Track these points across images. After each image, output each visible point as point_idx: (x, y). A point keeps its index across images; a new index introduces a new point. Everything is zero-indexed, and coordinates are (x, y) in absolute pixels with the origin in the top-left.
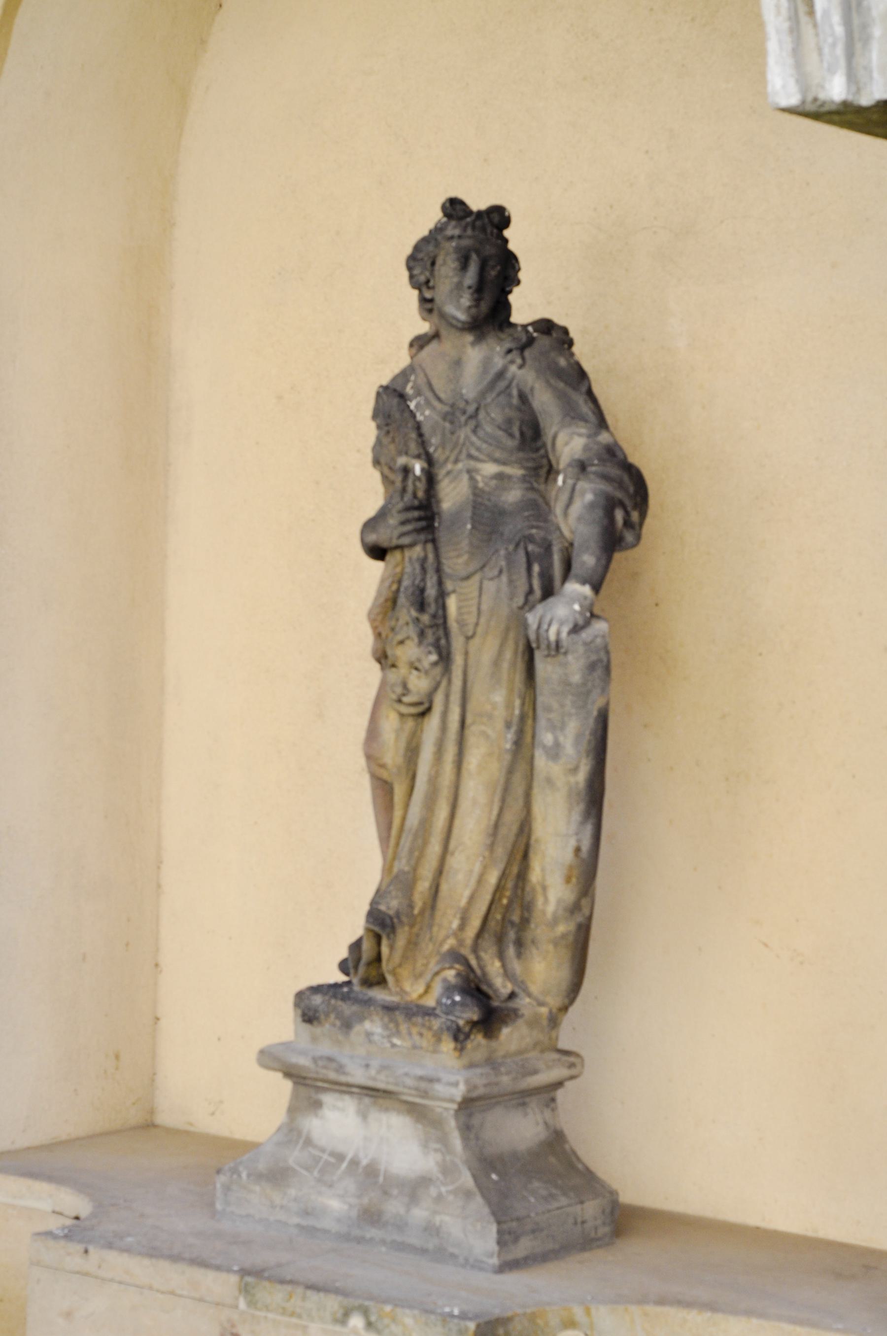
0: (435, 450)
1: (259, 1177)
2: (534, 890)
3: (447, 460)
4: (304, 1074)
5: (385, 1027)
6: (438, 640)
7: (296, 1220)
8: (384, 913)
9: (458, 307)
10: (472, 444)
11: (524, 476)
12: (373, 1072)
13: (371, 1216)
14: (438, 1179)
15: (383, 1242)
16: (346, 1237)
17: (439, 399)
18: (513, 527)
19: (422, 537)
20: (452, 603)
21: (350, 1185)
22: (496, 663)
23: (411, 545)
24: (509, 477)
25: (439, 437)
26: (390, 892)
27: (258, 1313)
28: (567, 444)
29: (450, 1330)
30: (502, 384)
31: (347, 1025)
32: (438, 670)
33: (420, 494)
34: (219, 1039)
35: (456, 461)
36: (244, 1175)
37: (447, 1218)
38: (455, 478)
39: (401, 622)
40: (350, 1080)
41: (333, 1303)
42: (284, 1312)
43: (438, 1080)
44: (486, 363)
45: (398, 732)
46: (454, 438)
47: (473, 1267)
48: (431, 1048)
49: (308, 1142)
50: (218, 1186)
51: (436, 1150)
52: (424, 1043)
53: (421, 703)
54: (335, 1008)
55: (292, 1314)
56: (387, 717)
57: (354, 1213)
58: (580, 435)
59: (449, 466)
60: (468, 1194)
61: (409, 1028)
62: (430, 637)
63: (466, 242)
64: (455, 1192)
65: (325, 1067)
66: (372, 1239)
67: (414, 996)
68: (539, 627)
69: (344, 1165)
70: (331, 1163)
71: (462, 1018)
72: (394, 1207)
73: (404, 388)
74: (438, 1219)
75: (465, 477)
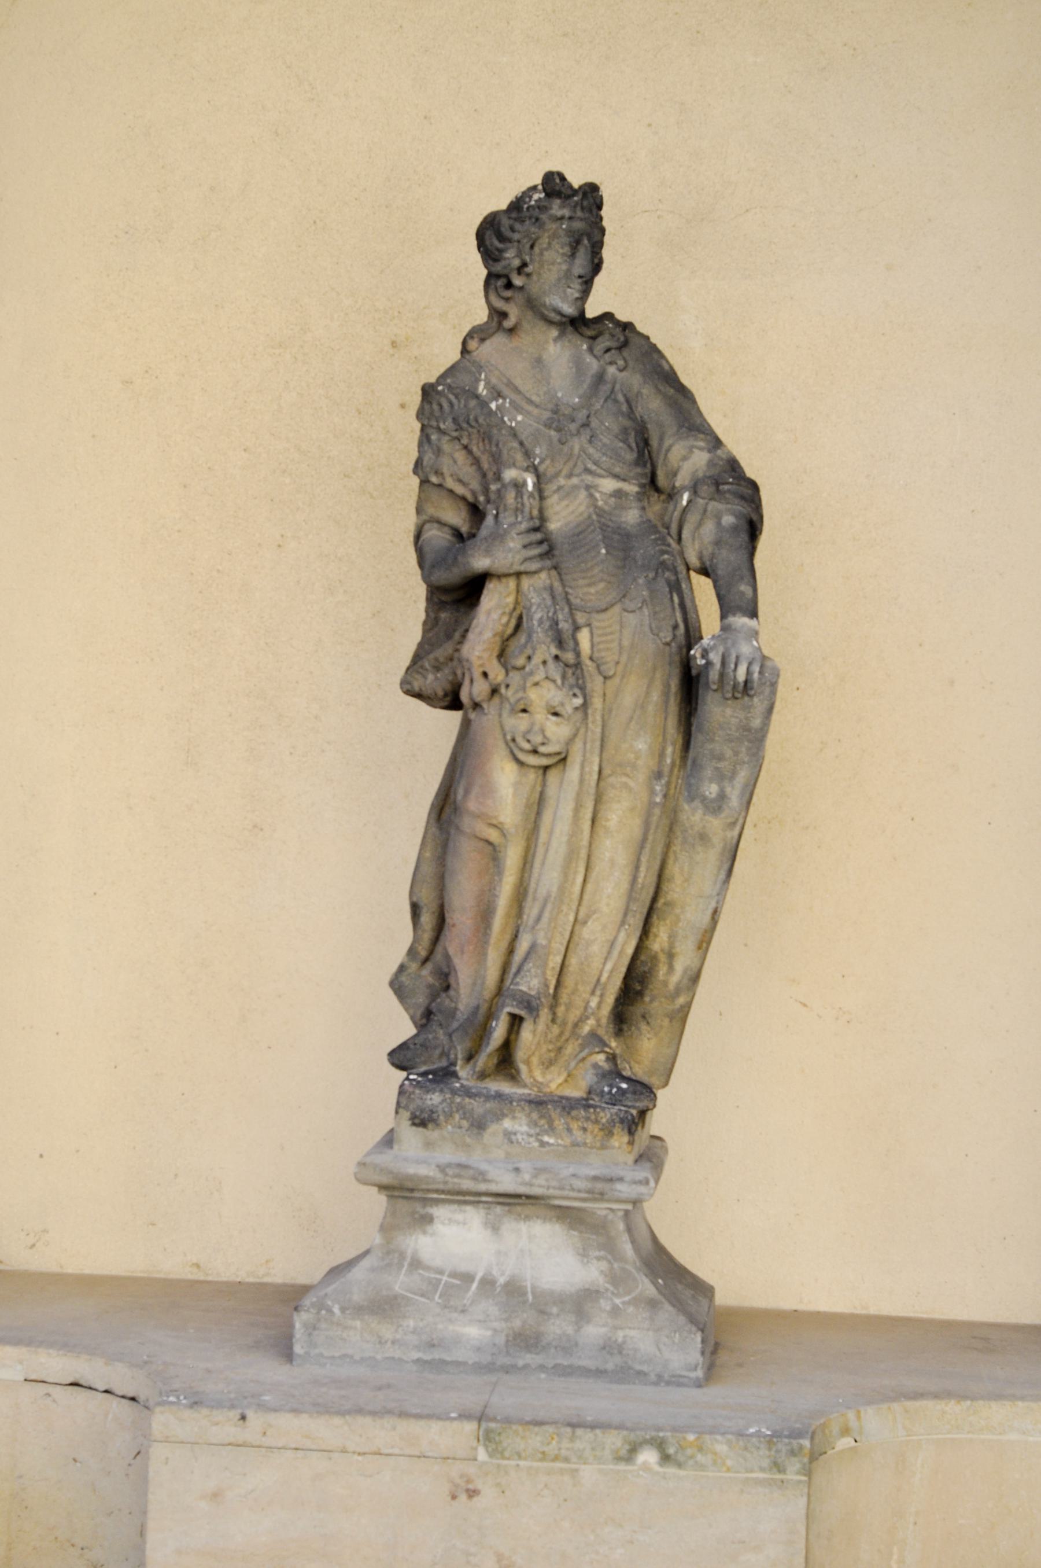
0: (542, 462)
1: (359, 1310)
2: (654, 958)
3: (557, 475)
4: (410, 1185)
7: (415, 1355)
8: (525, 993)
9: (564, 299)
10: (589, 456)
11: (638, 493)
12: (527, 1177)
13: (526, 1340)
14: (607, 1290)
15: (542, 1368)
16: (489, 1368)
17: (530, 402)
18: (644, 550)
19: (548, 563)
20: (584, 637)
21: (490, 1307)
22: (641, 706)
23: (535, 572)
24: (627, 494)
25: (544, 447)
26: (529, 971)
27: (505, 1462)
28: (685, 458)
29: (778, 1451)
31: (479, 1126)
34: (41, 1156)
35: (570, 476)
36: (336, 1310)
37: (632, 1333)
38: (568, 494)
39: (537, 660)
40: (494, 1188)
41: (614, 1441)
42: (544, 1456)
43: (621, 1179)
45: (517, 785)
46: (565, 448)
47: (668, 1383)
48: (598, 1144)
49: (416, 1264)
50: (298, 1325)
51: (598, 1259)
52: (589, 1139)
53: (559, 753)
54: (461, 1107)
55: (556, 1458)
56: (502, 769)
57: (501, 1340)
58: (701, 449)
59: (562, 481)
61: (567, 1124)
63: (578, 225)
65: (458, 1176)
66: (526, 1366)
67: (553, 1086)
68: (724, 663)
69: (475, 1285)
71: (634, 1107)
72: (559, 1326)
73: (477, 388)
74: (620, 1335)
75: (583, 494)
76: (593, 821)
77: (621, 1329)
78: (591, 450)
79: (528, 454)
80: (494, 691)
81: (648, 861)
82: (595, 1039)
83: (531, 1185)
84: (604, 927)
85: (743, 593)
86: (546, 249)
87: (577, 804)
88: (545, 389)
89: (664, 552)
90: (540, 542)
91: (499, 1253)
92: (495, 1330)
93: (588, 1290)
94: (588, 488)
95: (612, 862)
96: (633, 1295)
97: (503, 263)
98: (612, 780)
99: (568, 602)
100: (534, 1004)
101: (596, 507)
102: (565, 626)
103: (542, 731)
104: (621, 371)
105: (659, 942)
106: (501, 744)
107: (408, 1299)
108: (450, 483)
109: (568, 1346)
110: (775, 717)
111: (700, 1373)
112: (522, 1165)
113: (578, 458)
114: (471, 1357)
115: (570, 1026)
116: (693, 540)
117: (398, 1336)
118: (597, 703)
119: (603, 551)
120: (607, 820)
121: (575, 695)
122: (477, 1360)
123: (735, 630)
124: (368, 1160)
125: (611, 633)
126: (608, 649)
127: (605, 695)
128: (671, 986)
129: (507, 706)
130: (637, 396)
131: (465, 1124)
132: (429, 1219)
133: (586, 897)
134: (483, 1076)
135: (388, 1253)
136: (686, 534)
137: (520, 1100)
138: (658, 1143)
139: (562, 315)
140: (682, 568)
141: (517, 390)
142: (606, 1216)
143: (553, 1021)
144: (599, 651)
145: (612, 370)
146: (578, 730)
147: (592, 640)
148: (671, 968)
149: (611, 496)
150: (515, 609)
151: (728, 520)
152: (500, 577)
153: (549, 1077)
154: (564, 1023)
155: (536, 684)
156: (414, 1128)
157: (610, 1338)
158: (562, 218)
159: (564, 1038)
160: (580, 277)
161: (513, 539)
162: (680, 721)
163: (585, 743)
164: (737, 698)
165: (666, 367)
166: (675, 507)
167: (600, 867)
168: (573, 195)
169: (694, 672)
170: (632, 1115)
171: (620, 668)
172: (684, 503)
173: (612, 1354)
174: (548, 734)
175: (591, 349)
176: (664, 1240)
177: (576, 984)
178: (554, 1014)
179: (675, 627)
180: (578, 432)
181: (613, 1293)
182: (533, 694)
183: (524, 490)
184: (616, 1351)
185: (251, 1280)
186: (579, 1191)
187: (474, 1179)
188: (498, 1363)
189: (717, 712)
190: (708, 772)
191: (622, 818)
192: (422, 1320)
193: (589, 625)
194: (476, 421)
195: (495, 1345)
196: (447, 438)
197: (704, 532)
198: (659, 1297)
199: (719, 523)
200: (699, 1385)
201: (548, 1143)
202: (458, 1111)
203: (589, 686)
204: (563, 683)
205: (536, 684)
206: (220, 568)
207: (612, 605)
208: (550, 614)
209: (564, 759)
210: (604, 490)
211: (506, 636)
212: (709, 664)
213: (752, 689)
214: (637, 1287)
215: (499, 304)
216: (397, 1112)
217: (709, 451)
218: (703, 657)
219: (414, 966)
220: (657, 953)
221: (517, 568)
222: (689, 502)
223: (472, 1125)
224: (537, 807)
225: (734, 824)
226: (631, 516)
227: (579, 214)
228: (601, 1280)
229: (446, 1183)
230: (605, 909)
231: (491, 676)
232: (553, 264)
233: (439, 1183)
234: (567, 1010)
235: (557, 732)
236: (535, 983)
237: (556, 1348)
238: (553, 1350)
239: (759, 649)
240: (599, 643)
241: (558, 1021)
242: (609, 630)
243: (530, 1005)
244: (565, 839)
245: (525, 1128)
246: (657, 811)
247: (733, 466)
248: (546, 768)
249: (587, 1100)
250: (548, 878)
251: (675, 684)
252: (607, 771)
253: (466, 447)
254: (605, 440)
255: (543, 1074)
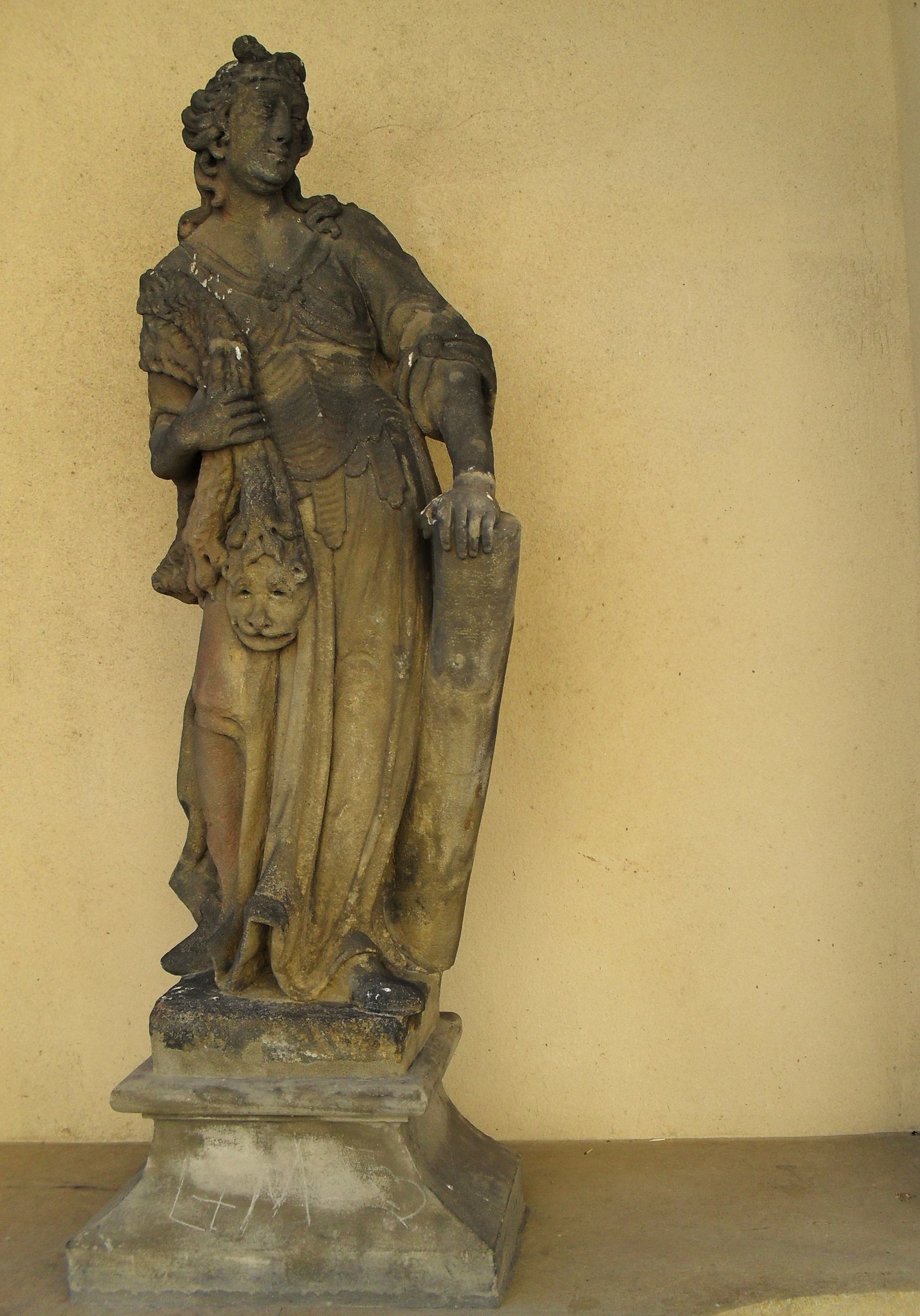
1: (131, 1244)
2: (421, 842)
3: (270, 342)
5: (292, 1039)
6: (300, 553)
7: (194, 1288)
12: (289, 1098)
13: (306, 1268)
14: (389, 1207)
15: (327, 1295)
17: (240, 274)
19: (261, 432)
20: (307, 510)
21: (266, 1233)
23: (248, 443)
24: (348, 359)
26: (274, 874)
28: (408, 320)
30: (319, 256)
31: (236, 1044)
32: (305, 592)
33: (246, 382)
35: (283, 342)
36: (108, 1245)
37: (419, 1255)
43: (389, 1095)
44: (291, 237)
45: (248, 674)
46: (277, 315)
47: (463, 1305)
49: (190, 1188)
50: (71, 1262)
51: (378, 1174)
57: (281, 1268)
58: (424, 309)
59: (275, 349)
60: (438, 1221)
62: (293, 554)
63: (271, 85)
64: (418, 1220)
66: (309, 1294)
67: (315, 993)
68: (454, 520)
69: (251, 1209)
70: (231, 1212)
71: (400, 1013)
72: (339, 1252)
75: (298, 361)
76: (335, 703)
77: (407, 1251)
78: (303, 315)
79: (237, 324)
80: (219, 576)
81: (397, 743)
82: (360, 939)
83: (294, 1107)
84: (357, 817)
85: (475, 448)
86: (242, 114)
87: (312, 689)
88: (256, 261)
89: (389, 414)
90: (252, 411)
91: (274, 1173)
92: (273, 1259)
93: (370, 1208)
94: (302, 353)
95: (360, 748)
96: (418, 1211)
97: (201, 135)
98: (350, 659)
99: (286, 471)
100: (281, 910)
101: (313, 372)
102: (283, 497)
103: (265, 612)
104: (335, 238)
105: (423, 824)
106: (229, 632)
107: (184, 1228)
108: (169, 368)
109: (352, 1272)
110: (521, 576)
111: (495, 1293)
112: (284, 1085)
113: (290, 324)
114: (252, 1288)
115: (330, 926)
116: (422, 400)
117: (174, 1270)
118: (326, 577)
119: (320, 415)
120: (349, 703)
121: (297, 570)
122: (258, 1290)
123: (467, 484)
124: (123, 1088)
125: (335, 501)
126: (333, 519)
127: (334, 568)
128: (442, 870)
129: (230, 589)
130: (354, 262)
131: (222, 1043)
132: (200, 1141)
133: (335, 786)
134: (241, 986)
135: (160, 1178)
136: (413, 395)
137: (277, 1014)
138: (447, 1024)
139: (268, 183)
140: (415, 437)
141: (227, 265)
142: (381, 1129)
143: (314, 920)
144: (323, 521)
145: (327, 238)
146: (305, 609)
147: (314, 511)
148: (439, 852)
149: (329, 360)
150: (232, 486)
151: (456, 376)
152: (215, 451)
153: (311, 982)
154: (323, 924)
155: (254, 562)
156: (169, 1049)
157: (395, 1263)
158: (254, 80)
159: (325, 938)
160: (279, 139)
161: (219, 409)
162: (418, 589)
163: (316, 623)
164: (473, 557)
165: (385, 233)
166: (401, 369)
167: (346, 754)
168: (267, 59)
169: (426, 534)
170: (397, 1023)
171: (348, 537)
172: (410, 364)
173: (399, 1278)
174: (272, 615)
175: (304, 222)
176: (466, 1110)
177: (333, 880)
178: (314, 913)
179: (406, 489)
180: (290, 298)
181: (396, 1210)
182: (252, 573)
183: (232, 359)
184: (403, 1275)
185: (116, 1141)
186: (347, 1110)
187: (234, 1103)
188: (281, 1292)
189: (454, 574)
190: (452, 642)
191: (364, 698)
192: (196, 1252)
193: (310, 495)
194: (186, 298)
195: (275, 1274)
196: (162, 323)
197: (434, 392)
198: (447, 1212)
199: (447, 382)
200: (496, 1305)
201: (310, 1057)
202: (212, 1029)
203: (316, 560)
204: (282, 559)
205: (254, 562)
206: (23, 499)
207: (334, 472)
208: (265, 485)
209: (295, 640)
210: (321, 355)
211: (226, 517)
212: (440, 522)
213: (488, 545)
214: (422, 1202)
215: (207, 182)
216: (151, 1034)
217: (433, 311)
218: (434, 516)
219: (190, 864)
220: (423, 836)
221: (225, 440)
222: (415, 362)
223: (228, 1044)
224: (271, 697)
225: (488, 694)
226: (354, 381)
227: (273, 75)
228: (383, 1196)
229: (205, 1108)
230: (356, 798)
231: (213, 559)
232: (250, 127)
233: (198, 1108)
234: (327, 908)
235: (281, 611)
236: (281, 886)
237: (339, 1274)
238: (336, 1277)
239: (495, 502)
240: (322, 513)
241: (319, 921)
242: (332, 498)
243: (278, 913)
244: (301, 727)
245: (284, 1044)
246: (401, 688)
247: (460, 324)
248: (279, 651)
249: (350, 1006)
250: (288, 771)
251: (408, 550)
252: (344, 650)
253: (181, 330)
254: (319, 304)
255: (305, 980)
